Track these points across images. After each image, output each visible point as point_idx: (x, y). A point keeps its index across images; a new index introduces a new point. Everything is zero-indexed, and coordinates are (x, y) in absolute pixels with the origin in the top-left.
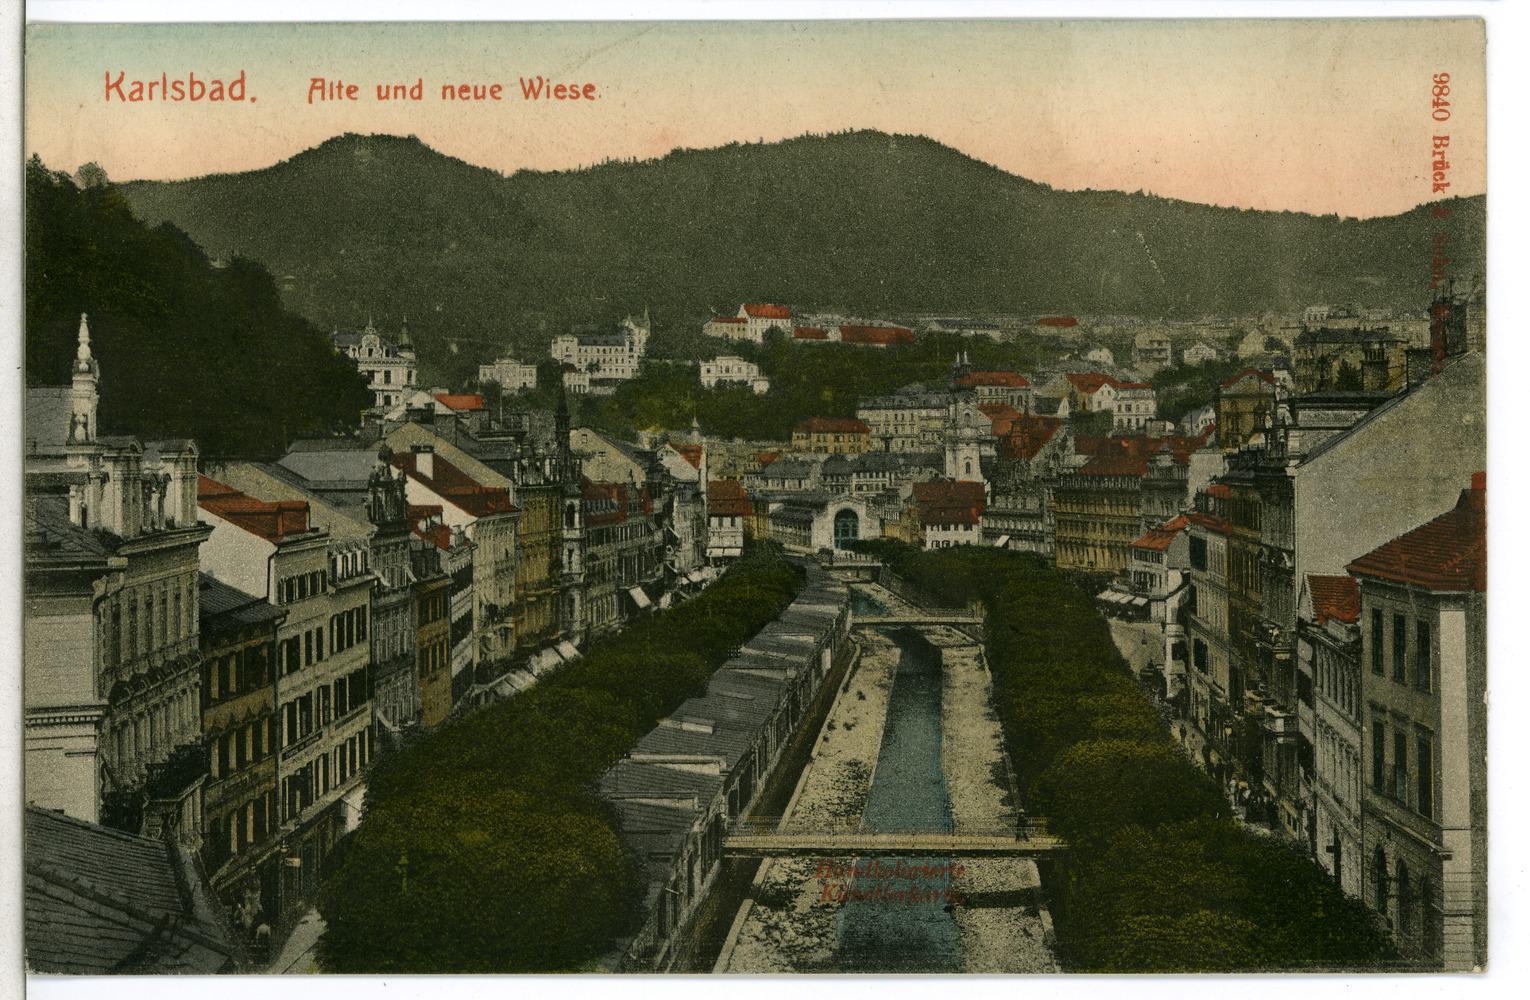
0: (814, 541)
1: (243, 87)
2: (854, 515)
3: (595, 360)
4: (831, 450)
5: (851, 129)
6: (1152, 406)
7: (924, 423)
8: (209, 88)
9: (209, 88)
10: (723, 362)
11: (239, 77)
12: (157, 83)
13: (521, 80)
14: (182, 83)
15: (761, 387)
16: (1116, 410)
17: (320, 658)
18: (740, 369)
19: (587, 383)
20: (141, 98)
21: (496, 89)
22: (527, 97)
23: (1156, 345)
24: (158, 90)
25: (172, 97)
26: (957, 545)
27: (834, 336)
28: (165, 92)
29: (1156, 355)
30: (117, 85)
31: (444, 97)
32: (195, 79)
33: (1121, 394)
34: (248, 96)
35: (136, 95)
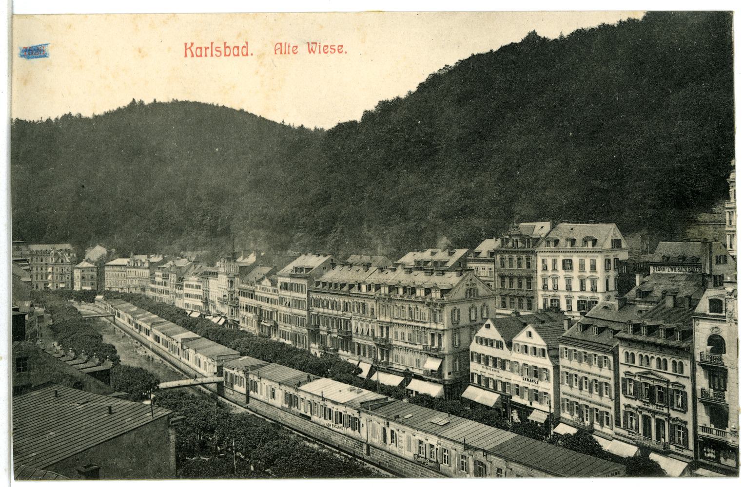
30: (190, 48)
32: (227, 45)
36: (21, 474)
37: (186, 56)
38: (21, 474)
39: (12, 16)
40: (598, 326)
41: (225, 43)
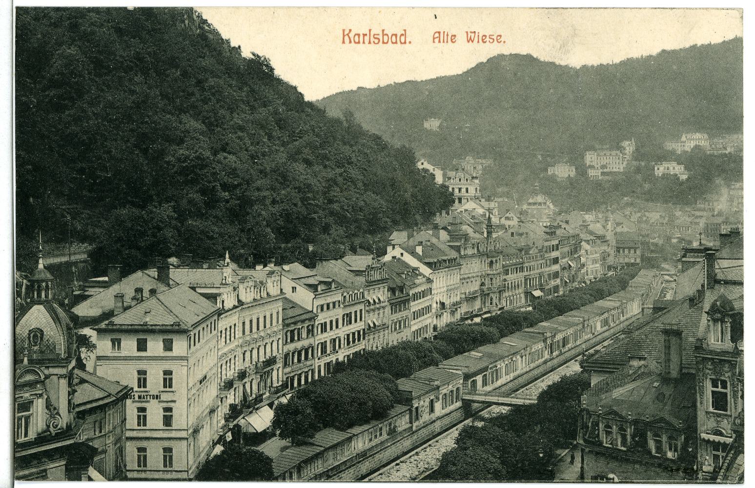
3: (605, 163)
5: (379, 86)
10: (665, 165)
17: (337, 327)
19: (600, 174)
21: (484, 38)
22: (468, 42)
24: (367, 38)
30: (348, 35)
31: (434, 42)
34: (407, 42)
41: (383, 31)
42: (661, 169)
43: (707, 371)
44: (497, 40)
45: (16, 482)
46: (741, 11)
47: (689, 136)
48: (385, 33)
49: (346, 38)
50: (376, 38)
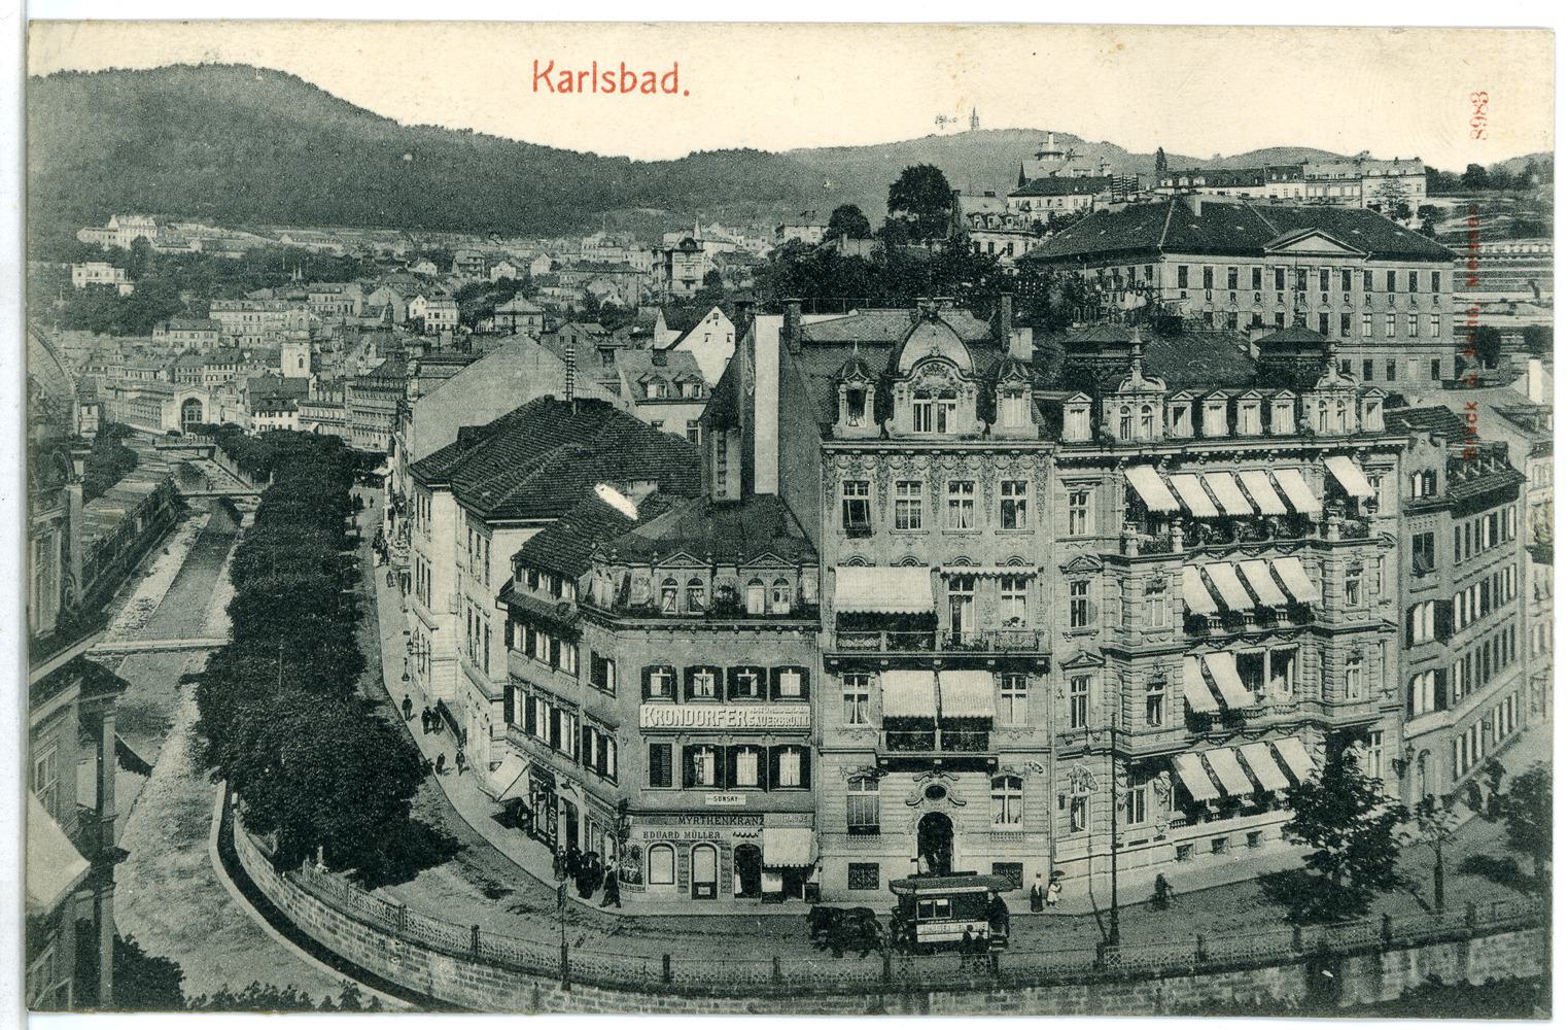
0: (164, 424)
1: (676, 80)
2: (198, 402)
4: (187, 345)
6: (455, 313)
7: (269, 324)
8: (641, 80)
9: (641, 80)
11: (672, 69)
12: (587, 73)
13: (536, 62)
14: (613, 74)
15: (126, 289)
16: (427, 317)
18: (108, 274)
20: (654, 90)
23: (472, 261)
24: (587, 81)
25: (603, 88)
26: (281, 429)
27: (195, 247)
28: (595, 82)
29: (472, 268)
30: (545, 74)
32: (626, 70)
33: (432, 304)
34: (681, 91)
35: (648, 87)
36: (42, 996)
37: (595, 90)
38: (42, 996)
39: (28, 25)
40: (1446, 712)
41: (623, 66)
42: (83, 272)
43: (839, 470)
44: (653, 81)
45: (739, 782)
46: (1546, 31)
47: (123, 220)
48: (626, 70)
49: (542, 82)
50: (611, 82)
